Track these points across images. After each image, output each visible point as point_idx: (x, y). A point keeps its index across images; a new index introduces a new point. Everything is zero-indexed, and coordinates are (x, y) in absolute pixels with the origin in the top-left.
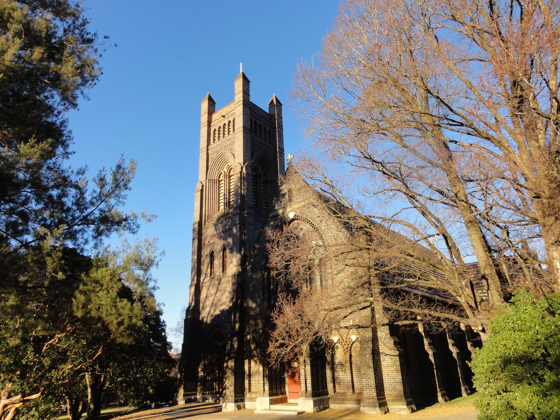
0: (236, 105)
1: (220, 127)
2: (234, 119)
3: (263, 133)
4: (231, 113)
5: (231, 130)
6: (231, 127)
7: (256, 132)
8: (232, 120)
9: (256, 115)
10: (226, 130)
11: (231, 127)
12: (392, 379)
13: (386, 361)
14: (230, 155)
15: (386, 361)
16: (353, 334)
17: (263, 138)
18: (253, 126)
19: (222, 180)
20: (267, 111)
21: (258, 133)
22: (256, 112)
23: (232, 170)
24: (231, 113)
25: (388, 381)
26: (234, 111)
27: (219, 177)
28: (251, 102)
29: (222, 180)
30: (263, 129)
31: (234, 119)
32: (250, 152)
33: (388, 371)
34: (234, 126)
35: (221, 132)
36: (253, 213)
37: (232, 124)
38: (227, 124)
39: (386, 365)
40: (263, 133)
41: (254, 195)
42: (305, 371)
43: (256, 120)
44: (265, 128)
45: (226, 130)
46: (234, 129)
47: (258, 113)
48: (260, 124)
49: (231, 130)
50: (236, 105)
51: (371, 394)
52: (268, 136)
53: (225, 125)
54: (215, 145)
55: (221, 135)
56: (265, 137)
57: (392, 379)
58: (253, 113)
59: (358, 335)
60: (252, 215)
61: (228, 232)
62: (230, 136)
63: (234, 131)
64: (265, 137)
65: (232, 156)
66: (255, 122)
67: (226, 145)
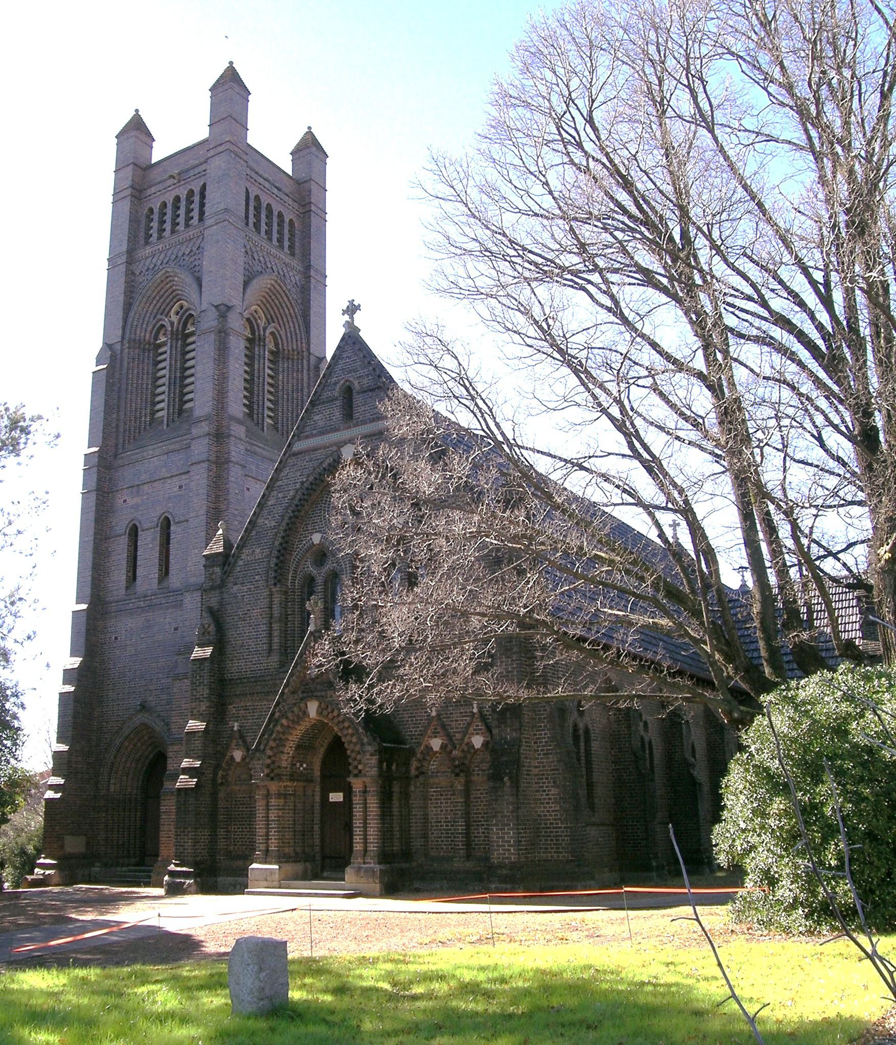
0: (212, 153)
1: (164, 205)
2: (204, 188)
3: (275, 227)
4: (197, 171)
5: (195, 214)
6: (196, 206)
7: (257, 226)
8: (197, 190)
9: (261, 180)
10: (182, 211)
11: (196, 206)
12: (561, 836)
13: (544, 791)
14: (189, 280)
15: (544, 791)
16: (477, 734)
17: (275, 242)
18: (251, 208)
19: (164, 344)
20: (287, 167)
21: (264, 227)
22: (261, 172)
23: (191, 321)
24: (197, 171)
25: (546, 832)
26: (203, 167)
27: (156, 337)
28: (249, 145)
29: (164, 344)
30: (275, 219)
31: (204, 188)
32: (92, 516)
33: (548, 811)
34: (202, 205)
35: (168, 218)
36: (243, 436)
37: (197, 198)
38: (183, 197)
39: (545, 799)
40: (275, 227)
41: (245, 389)
42: (365, 843)
43: (258, 192)
44: (280, 215)
45: (182, 211)
46: (202, 213)
47: (266, 176)
48: (269, 205)
49: (195, 214)
50: (212, 153)
51: (507, 858)
52: (286, 236)
53: (177, 199)
54: (175, 238)
55: (168, 226)
56: (280, 240)
57: (561, 836)
58: (253, 175)
59: (488, 734)
60: (241, 440)
61: (175, 479)
62: (192, 232)
63: (201, 219)
64: (280, 240)
65: (195, 286)
66: (257, 198)
67: (180, 254)
